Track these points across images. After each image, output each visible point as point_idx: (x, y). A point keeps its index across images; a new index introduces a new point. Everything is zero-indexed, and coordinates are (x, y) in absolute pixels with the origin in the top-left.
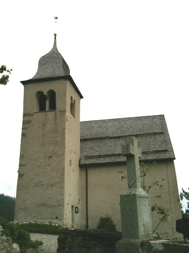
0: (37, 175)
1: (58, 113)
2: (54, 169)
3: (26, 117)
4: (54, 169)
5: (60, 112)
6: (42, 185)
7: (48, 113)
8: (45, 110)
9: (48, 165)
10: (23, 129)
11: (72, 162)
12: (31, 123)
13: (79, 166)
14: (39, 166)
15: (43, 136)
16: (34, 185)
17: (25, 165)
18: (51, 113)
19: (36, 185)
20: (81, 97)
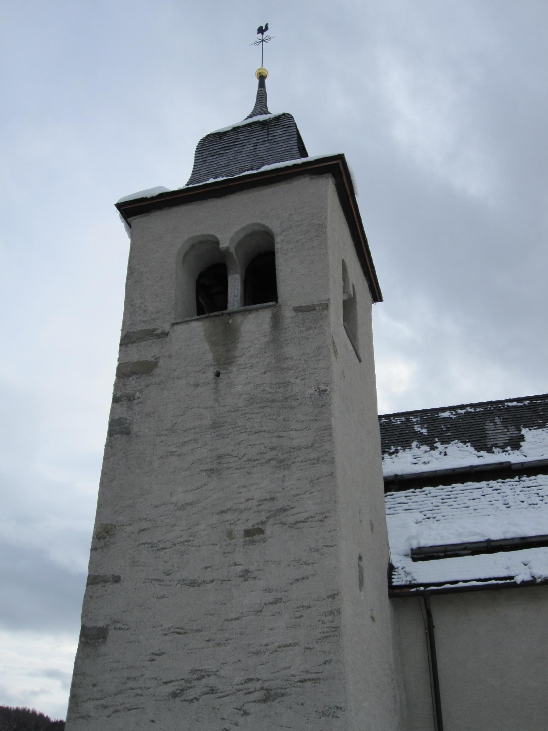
0: (180, 632)
1: (288, 314)
2: (277, 601)
3: (133, 348)
4: (277, 601)
5: (298, 310)
6: (212, 691)
7: (239, 318)
8: (226, 308)
9: (246, 575)
10: (116, 400)
11: (365, 563)
12: (157, 371)
13: (391, 596)
14: (193, 583)
15: (215, 425)
16: (170, 688)
17: (117, 579)
18: (251, 317)
19: (174, 695)
20: (377, 296)
